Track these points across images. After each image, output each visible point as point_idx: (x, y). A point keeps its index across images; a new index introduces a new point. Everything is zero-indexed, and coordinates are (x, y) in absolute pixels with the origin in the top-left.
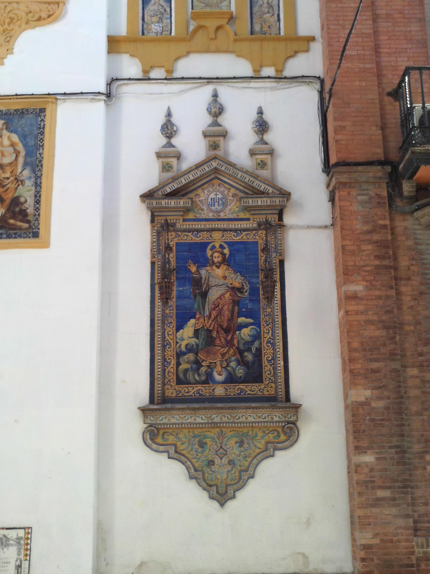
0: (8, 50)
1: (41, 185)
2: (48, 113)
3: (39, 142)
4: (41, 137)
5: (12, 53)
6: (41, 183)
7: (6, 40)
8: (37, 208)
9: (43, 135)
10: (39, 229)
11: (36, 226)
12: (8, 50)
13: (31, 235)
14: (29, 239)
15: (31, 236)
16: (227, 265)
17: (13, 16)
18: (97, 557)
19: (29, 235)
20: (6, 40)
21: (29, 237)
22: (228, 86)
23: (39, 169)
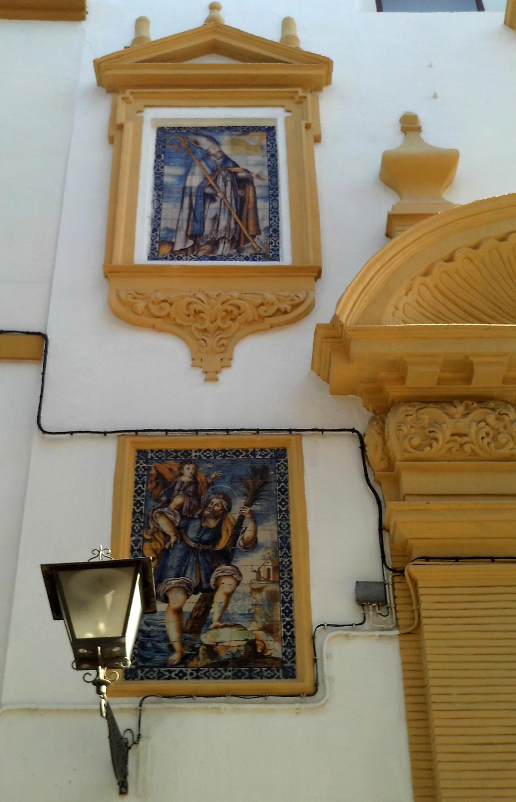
0: (222, 359)
1: (387, 420)
2: (291, 455)
3: (278, 506)
4: (283, 497)
5: (229, 366)
6: (291, 578)
7: (220, 343)
8: (288, 623)
9: (286, 493)
10: (294, 662)
11: (290, 657)
12: (222, 359)
13: (280, 673)
14: (278, 680)
15: (281, 676)
16: (189, 509)
17: (230, 308)
18: (184, 127)
19: (278, 674)
20: (220, 343)
21: (278, 678)
22: (401, 568)
23: (285, 553)
